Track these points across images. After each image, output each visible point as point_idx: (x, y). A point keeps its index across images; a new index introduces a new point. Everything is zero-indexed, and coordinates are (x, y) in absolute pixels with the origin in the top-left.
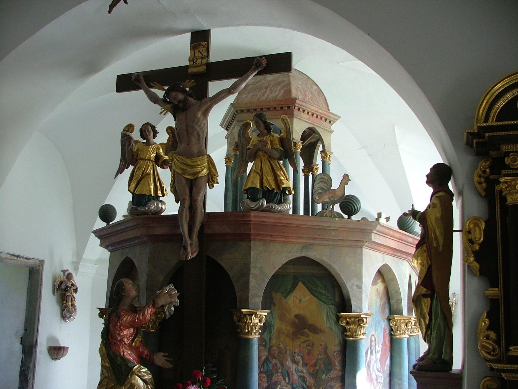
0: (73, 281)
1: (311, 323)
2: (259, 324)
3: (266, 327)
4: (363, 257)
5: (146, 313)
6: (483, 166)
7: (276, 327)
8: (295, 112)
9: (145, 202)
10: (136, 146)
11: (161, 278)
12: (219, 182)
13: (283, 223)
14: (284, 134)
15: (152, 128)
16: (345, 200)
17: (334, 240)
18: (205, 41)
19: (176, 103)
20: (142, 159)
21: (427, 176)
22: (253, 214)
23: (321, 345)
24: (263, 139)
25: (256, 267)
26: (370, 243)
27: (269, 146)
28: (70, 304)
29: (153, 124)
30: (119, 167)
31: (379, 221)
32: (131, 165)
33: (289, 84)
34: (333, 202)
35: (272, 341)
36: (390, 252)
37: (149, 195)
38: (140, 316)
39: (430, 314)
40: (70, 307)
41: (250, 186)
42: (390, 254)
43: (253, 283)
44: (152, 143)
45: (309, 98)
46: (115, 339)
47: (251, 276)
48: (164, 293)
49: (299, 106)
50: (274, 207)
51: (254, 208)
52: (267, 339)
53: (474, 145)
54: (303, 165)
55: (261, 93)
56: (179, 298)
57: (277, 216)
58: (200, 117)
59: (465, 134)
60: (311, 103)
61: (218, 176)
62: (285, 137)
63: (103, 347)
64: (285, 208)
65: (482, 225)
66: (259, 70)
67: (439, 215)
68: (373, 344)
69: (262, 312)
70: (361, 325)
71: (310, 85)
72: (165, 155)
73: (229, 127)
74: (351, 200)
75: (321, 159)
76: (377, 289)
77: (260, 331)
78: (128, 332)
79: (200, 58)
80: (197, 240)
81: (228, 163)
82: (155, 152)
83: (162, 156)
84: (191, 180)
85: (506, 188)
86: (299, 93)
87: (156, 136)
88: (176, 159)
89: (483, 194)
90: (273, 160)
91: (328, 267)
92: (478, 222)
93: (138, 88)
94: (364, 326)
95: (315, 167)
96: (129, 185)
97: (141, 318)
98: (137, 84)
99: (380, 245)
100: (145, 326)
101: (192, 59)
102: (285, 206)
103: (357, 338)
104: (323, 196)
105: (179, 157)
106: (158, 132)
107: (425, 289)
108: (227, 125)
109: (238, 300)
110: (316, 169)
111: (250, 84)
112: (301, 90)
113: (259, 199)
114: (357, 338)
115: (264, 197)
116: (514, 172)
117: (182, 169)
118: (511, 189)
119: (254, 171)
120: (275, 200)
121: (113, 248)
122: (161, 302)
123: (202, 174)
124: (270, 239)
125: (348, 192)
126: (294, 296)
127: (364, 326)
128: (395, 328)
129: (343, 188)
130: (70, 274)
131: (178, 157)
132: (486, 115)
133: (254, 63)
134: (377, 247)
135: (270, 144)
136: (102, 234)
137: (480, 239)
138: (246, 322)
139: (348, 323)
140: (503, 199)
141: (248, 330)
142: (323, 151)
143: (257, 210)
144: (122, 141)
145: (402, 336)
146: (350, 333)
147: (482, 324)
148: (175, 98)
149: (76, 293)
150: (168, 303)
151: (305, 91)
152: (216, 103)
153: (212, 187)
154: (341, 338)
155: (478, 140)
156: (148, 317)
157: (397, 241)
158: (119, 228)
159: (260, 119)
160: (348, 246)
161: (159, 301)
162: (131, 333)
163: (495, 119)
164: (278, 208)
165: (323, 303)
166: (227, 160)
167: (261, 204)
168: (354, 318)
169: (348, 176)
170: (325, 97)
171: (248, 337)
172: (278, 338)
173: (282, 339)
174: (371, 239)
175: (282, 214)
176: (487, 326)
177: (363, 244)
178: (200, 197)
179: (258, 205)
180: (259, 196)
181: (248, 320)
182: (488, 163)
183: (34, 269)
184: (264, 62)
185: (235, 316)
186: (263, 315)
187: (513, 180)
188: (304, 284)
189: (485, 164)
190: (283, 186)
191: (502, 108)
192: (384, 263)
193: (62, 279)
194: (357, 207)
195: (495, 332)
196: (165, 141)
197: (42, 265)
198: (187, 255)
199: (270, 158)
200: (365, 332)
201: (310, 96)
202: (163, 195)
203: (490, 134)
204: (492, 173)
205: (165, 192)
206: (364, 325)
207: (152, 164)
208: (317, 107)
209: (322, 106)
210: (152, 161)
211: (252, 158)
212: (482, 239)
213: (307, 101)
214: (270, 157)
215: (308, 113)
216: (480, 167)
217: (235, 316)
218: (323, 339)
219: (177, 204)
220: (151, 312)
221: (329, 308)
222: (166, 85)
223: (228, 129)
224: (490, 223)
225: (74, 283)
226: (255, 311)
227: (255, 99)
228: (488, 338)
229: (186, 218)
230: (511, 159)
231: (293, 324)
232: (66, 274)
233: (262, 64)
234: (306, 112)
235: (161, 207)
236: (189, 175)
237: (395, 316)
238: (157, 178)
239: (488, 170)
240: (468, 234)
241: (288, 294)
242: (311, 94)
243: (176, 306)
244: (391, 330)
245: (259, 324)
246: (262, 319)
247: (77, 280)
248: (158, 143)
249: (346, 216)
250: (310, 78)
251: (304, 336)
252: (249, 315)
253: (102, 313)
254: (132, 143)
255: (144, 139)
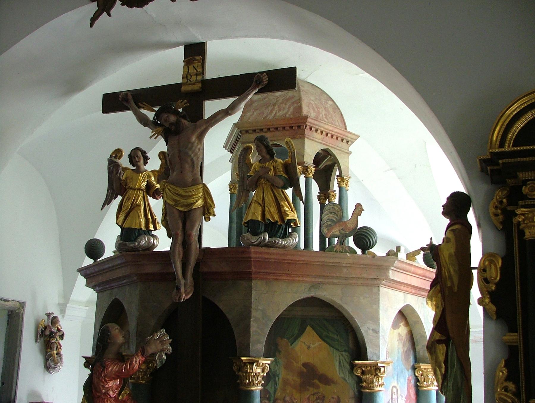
0: (59, 326)
1: (321, 373)
2: (262, 374)
3: (270, 378)
4: (380, 296)
5: (134, 362)
6: (499, 196)
7: (281, 376)
8: (307, 132)
9: (135, 237)
10: (125, 173)
11: (153, 322)
12: (216, 214)
13: (288, 260)
14: (289, 160)
15: (142, 154)
16: (358, 233)
17: (346, 278)
18: (200, 56)
19: (168, 126)
20: (131, 189)
21: (443, 206)
22: (253, 250)
23: (333, 398)
24: (266, 165)
25: (257, 310)
26: (388, 281)
27: (271, 173)
28: (55, 352)
29: (144, 149)
30: (105, 197)
31: (398, 256)
32: (119, 195)
33: (300, 100)
34: (344, 235)
35: (276, 393)
36: (413, 291)
37: (139, 229)
38: (128, 365)
39: (446, 362)
40: (56, 356)
41: (249, 219)
42: (413, 294)
43: (254, 326)
44: (142, 169)
45: (322, 115)
46: (99, 392)
47: (252, 319)
48: (154, 339)
49: (311, 125)
50: (277, 242)
51: (255, 243)
52: (272, 391)
53: (489, 172)
54: (319, 192)
55: (267, 111)
56: (171, 344)
57: (280, 251)
58: (194, 142)
59: (478, 160)
60: (325, 121)
61: (214, 208)
62: (290, 162)
63: (85, 400)
64: (290, 243)
65: (498, 262)
66: (260, 88)
67: (452, 251)
68: (395, 396)
69: (265, 360)
70: (378, 375)
71: (324, 101)
72: (158, 184)
73: (233, 149)
74: (366, 232)
75: (338, 185)
76: (399, 333)
77: (263, 382)
78: (114, 383)
79: (194, 75)
80: (192, 279)
81: (232, 190)
82: (146, 181)
83: (154, 185)
84: (185, 213)
85: (524, 220)
86: (312, 110)
87: (147, 163)
88: (168, 188)
89: (500, 227)
90: (277, 188)
91: (340, 309)
92: (493, 259)
93: (126, 109)
94: (382, 375)
95: (332, 193)
96: (117, 218)
97: (129, 367)
98: (125, 104)
99: (401, 284)
100: (135, 377)
101: (186, 75)
102: (290, 240)
103: (373, 389)
104: (332, 229)
105: (172, 186)
106: (149, 158)
107: (439, 334)
108: (231, 147)
109: (238, 347)
110: (333, 195)
111: (256, 101)
112: (313, 107)
113: (261, 233)
114: (373, 389)
115: (266, 230)
116: (532, 203)
117: (175, 201)
118: (528, 222)
119: (256, 201)
120: (279, 233)
121: (99, 288)
122: (151, 350)
123: (197, 206)
124: (274, 277)
125: (362, 222)
126: (301, 342)
127: (382, 375)
128: (421, 378)
129: (355, 219)
130: (55, 318)
131: (170, 187)
132: (501, 139)
133: (255, 80)
134: (397, 285)
135: (273, 171)
136: (88, 272)
137: (496, 278)
138: (246, 372)
139: (363, 373)
140: (522, 233)
141: (249, 381)
142: (340, 176)
143: (258, 245)
144: (109, 169)
145: (429, 388)
146: (366, 384)
147: (499, 374)
148: (166, 121)
149: (62, 339)
150: (159, 350)
151: (318, 108)
152: (212, 125)
153: (208, 220)
154: (356, 390)
155: (492, 168)
156: (136, 366)
157: (421, 278)
158: (107, 266)
159: (261, 143)
160: (362, 285)
161: (148, 349)
162: (117, 385)
163: (511, 144)
164: (282, 243)
165: (334, 350)
166: (231, 187)
167: (262, 238)
168: (370, 366)
169: (361, 205)
170: (342, 114)
171: (249, 388)
172: (284, 390)
173: (288, 391)
174: (389, 276)
175: (286, 249)
176: (505, 376)
177: (379, 283)
178: (194, 231)
179: (260, 239)
180: (260, 230)
181: (249, 369)
182: (505, 192)
183: (14, 312)
184: (265, 79)
185: (234, 365)
186: (266, 364)
187: (529, 212)
188: (314, 328)
189: (502, 193)
190: (287, 218)
191: (520, 131)
192: (406, 304)
193: (46, 324)
194: (373, 241)
195: (514, 383)
196: (158, 168)
197: (23, 307)
198: (180, 297)
199: (273, 186)
200: (383, 383)
201: (324, 113)
202: (155, 229)
203: (504, 161)
204: (509, 203)
205: (157, 226)
206: (381, 374)
207: (142, 194)
208: (331, 126)
209: (338, 124)
210: (142, 190)
211: (253, 187)
212: (498, 278)
213: (321, 120)
214: (273, 185)
215: (322, 133)
216: (497, 197)
217: (234, 365)
218: (336, 391)
219: (169, 239)
220: (140, 360)
221: (342, 355)
222: (156, 106)
223: (233, 151)
224: (507, 260)
225: (60, 328)
226: (256, 359)
227: (261, 117)
228: (506, 389)
229: (179, 254)
230: (529, 188)
231: (301, 374)
232: (51, 317)
233: (262, 81)
234: (319, 131)
235: (153, 242)
236: (182, 206)
237: (421, 364)
238: (148, 210)
239: (505, 200)
240: (483, 273)
241: (296, 339)
242: (326, 111)
243: (168, 354)
244: (417, 380)
245: (262, 374)
246: (265, 368)
247: (64, 324)
248: (149, 170)
249: (359, 251)
250: (324, 92)
251: (313, 387)
252: (249, 363)
253: (88, 362)
254: (120, 171)
255: (133, 166)
